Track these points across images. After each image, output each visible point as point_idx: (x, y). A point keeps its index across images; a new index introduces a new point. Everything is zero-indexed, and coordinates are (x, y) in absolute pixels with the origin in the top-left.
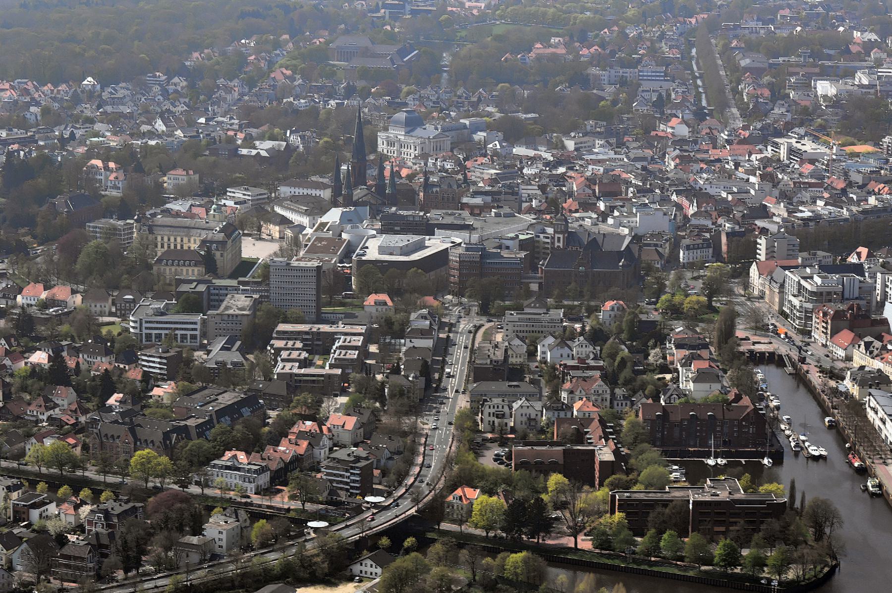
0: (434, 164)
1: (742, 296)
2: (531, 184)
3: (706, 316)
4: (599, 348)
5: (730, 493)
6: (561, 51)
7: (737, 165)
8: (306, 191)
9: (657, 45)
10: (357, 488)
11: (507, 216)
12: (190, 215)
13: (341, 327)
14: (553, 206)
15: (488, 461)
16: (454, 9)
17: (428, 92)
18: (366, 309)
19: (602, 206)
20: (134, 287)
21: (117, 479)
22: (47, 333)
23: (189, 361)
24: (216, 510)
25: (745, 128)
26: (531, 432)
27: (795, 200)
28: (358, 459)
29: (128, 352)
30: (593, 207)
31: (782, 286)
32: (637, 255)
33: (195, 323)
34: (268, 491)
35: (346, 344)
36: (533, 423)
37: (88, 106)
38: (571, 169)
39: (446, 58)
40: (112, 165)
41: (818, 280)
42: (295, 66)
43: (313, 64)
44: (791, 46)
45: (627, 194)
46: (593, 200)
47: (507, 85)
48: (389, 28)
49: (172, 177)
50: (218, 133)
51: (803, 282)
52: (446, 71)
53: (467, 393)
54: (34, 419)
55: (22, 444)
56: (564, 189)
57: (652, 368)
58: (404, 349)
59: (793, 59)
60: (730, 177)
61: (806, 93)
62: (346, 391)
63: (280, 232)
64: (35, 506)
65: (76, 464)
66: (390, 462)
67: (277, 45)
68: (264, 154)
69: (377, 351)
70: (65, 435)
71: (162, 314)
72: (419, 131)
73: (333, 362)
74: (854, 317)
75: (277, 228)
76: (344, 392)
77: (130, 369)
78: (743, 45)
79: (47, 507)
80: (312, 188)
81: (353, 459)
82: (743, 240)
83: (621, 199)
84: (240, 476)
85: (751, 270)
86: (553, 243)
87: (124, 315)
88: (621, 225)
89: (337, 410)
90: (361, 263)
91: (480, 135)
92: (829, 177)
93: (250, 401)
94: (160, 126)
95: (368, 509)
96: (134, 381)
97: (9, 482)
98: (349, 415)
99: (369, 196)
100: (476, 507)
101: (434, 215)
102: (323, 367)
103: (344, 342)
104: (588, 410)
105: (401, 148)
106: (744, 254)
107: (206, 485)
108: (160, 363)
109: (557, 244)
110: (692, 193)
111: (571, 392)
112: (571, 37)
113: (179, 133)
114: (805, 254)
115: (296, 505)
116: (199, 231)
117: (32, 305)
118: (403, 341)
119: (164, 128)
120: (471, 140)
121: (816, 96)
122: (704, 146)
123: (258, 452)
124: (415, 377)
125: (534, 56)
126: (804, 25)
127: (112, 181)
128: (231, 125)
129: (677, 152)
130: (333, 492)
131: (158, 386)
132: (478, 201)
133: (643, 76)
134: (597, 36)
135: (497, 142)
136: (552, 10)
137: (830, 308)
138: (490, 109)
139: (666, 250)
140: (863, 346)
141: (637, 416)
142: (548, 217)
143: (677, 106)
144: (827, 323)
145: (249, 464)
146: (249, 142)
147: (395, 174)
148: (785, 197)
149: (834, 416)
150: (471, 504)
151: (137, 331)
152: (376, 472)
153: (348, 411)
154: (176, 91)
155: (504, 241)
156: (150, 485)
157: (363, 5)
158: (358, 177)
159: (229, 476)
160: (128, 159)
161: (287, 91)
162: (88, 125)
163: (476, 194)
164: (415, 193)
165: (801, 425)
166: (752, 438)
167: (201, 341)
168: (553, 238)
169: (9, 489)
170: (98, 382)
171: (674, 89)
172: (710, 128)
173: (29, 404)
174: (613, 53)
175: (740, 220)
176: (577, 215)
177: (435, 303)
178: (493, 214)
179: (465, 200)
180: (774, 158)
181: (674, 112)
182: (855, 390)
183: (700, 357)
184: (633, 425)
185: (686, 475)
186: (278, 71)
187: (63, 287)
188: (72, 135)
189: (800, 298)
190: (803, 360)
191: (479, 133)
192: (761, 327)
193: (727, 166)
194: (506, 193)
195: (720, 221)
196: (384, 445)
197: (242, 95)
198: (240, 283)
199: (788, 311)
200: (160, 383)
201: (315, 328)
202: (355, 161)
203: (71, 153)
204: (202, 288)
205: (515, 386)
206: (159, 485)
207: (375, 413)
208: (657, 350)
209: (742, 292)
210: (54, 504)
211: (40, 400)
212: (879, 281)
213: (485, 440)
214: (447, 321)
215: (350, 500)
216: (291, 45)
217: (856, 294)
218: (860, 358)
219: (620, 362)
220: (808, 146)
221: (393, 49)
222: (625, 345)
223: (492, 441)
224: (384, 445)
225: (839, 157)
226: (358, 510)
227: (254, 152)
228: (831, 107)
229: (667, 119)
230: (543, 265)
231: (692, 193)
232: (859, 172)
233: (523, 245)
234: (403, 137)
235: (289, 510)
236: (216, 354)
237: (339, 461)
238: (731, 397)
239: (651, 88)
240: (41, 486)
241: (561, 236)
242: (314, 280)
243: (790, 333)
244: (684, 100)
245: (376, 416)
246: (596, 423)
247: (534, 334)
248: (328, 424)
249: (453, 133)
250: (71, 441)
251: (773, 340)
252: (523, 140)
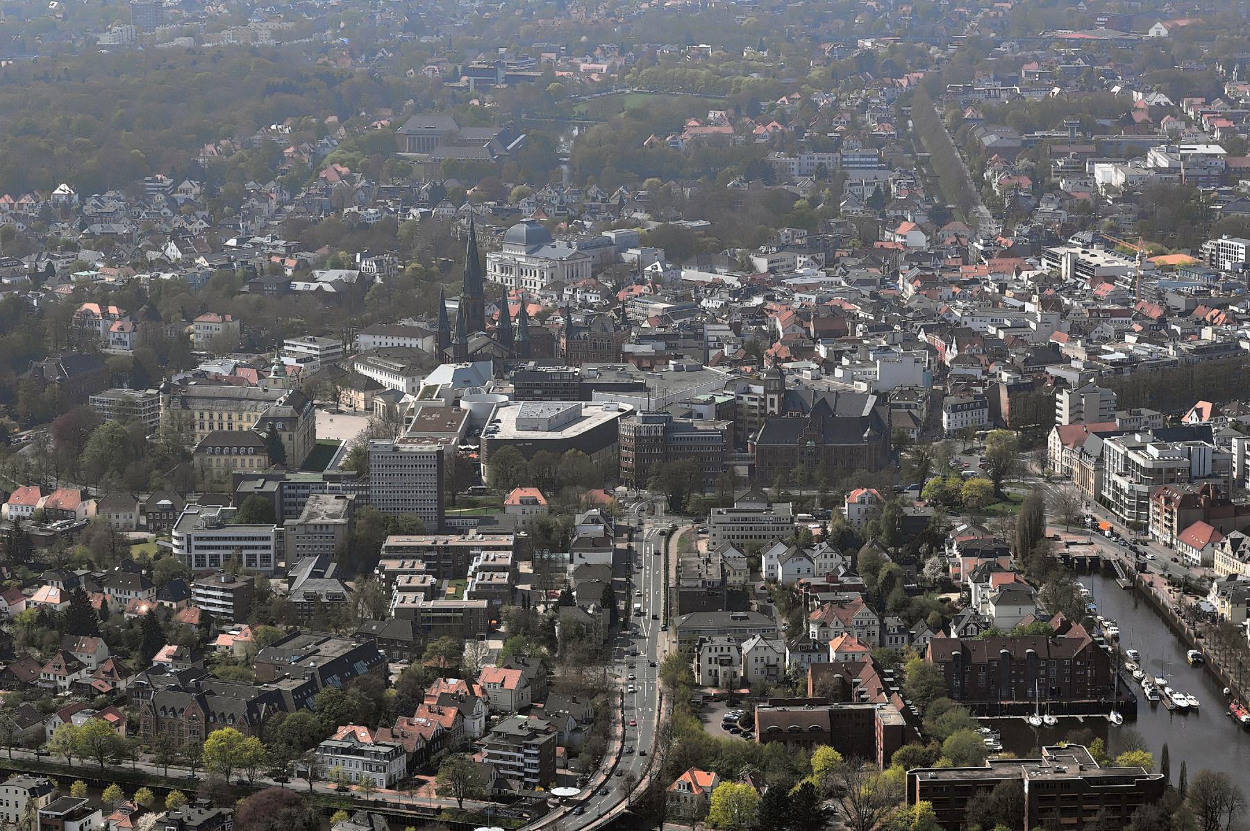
0: (572, 296)
1: (1039, 476)
2: (717, 323)
3: (992, 507)
4: (849, 558)
5: (1081, 768)
6: (727, 129)
7: (1003, 288)
8: (396, 341)
9: (859, 118)
10: (535, 776)
11: (690, 369)
12: (233, 380)
13: (473, 538)
14: (753, 353)
15: (715, 728)
16: (565, 73)
17: (546, 193)
18: (508, 510)
19: (822, 351)
20: (168, 487)
21: (186, 773)
22: (51, 559)
23: (264, 594)
24: (337, 815)
25: (1007, 233)
26: (776, 683)
27: (1093, 335)
28: (535, 733)
29: (174, 583)
30: (809, 353)
31: (1100, 460)
32: (886, 422)
33: (268, 538)
34: (405, 783)
35: (489, 562)
36: (773, 672)
37: (65, 225)
38: (770, 298)
39: (565, 147)
40: (113, 310)
41: (1153, 451)
42: (353, 160)
43: (377, 156)
44: (1050, 115)
45: (854, 333)
46: (809, 343)
47: (656, 179)
48: (476, 102)
49: (202, 325)
50: (257, 260)
51: (1131, 455)
52: (565, 163)
53: (671, 629)
54: (51, 686)
55: (40, 724)
56: (764, 327)
57: (928, 585)
58: (571, 568)
59: (1055, 134)
60: (995, 304)
61: (1083, 182)
62: (495, 632)
63: (366, 400)
64: (71, 817)
65: (122, 753)
66: (577, 735)
67: (323, 131)
68: (328, 288)
69: (531, 571)
70: (102, 709)
71: (219, 527)
72: (546, 251)
73: (474, 589)
74: (1211, 503)
75: (362, 395)
76: (492, 633)
77: (179, 610)
78: (981, 116)
79: (90, 817)
80: (405, 336)
81: (527, 733)
82: (1032, 395)
83: (849, 341)
84: (365, 763)
85: (1050, 439)
86: (764, 407)
87: (159, 528)
88: (853, 379)
89: (486, 660)
90: (495, 445)
91: (632, 254)
92: (1137, 303)
93: (367, 652)
94: (173, 252)
95: (557, 806)
96: (189, 625)
97: (33, 782)
98: (509, 667)
99: (491, 346)
100: (716, 799)
101: (586, 370)
102: (458, 597)
103: (487, 560)
104: (851, 649)
105: (523, 273)
106: (1034, 418)
107: (314, 778)
108: (223, 598)
109: (769, 409)
110: (949, 330)
111: (824, 625)
112: (737, 109)
113: (201, 261)
114: (1123, 414)
115: (451, 802)
116: (253, 403)
117: (24, 518)
118: (567, 556)
119: (179, 255)
120: (619, 260)
121: (1095, 185)
122: (950, 260)
123: (385, 726)
124: (597, 609)
125: (689, 138)
126: (1062, 85)
127: (117, 334)
128: (275, 247)
129: (916, 271)
130: (501, 782)
131: (224, 632)
132: (646, 348)
133: (848, 162)
134: (773, 107)
135: (658, 263)
136: (704, 72)
137: (1176, 491)
138: (638, 215)
139: (922, 414)
140: (1228, 545)
141: (922, 656)
142: (749, 369)
143: (902, 205)
144: (1171, 513)
145: (376, 744)
146: (304, 271)
147: (523, 315)
148: (1077, 331)
149: (1200, 649)
150: (706, 795)
151: (184, 552)
152: (560, 751)
153: (511, 659)
154: (188, 201)
155: (694, 407)
156: (234, 779)
157: (434, 71)
158: (473, 317)
159: (347, 762)
160: (133, 300)
161: (345, 198)
162: (70, 254)
163: (642, 339)
164: (551, 340)
165: (1154, 662)
166: (1092, 689)
167: (276, 564)
168: (764, 400)
169: (34, 792)
170: (138, 628)
171: (895, 181)
172: (956, 235)
173: (42, 665)
174: (800, 131)
175: (1022, 367)
176: (789, 365)
177: (608, 500)
178: (671, 368)
179: (628, 348)
180: (1052, 276)
181: (899, 213)
182: (1225, 610)
183: (999, 568)
184: (923, 672)
185: (1001, 740)
186: (330, 168)
187: (69, 491)
188: (50, 269)
189: (1129, 478)
190: (1142, 568)
191: (630, 251)
192: (1075, 522)
193: (986, 289)
194: (686, 337)
195: (993, 368)
196: (566, 710)
197: (282, 204)
198: (326, 478)
199: (1110, 497)
200: (225, 627)
201: (441, 540)
202: (468, 296)
203: (51, 294)
204: (272, 487)
205: (742, 618)
206: (246, 779)
207: (545, 663)
208: (935, 559)
209: (1039, 471)
210: (100, 812)
211: (59, 659)
212: (1235, 450)
213: (707, 697)
214: (624, 523)
215: (526, 793)
216: (342, 131)
217: (1208, 471)
218: (1224, 564)
219: (887, 578)
220: (1100, 258)
221: (492, 133)
222: (888, 552)
223: (718, 698)
224: (566, 710)
225: (1148, 273)
226: (541, 809)
227: (314, 286)
228: (1123, 200)
229: (896, 223)
230: (754, 439)
231: (949, 330)
232: (1180, 293)
233: (723, 411)
234: (523, 260)
235: (439, 811)
236: (303, 581)
237: (508, 737)
238: (1056, 624)
239: (863, 181)
240: (78, 787)
241: (776, 397)
242: (434, 470)
243: (1116, 529)
244: (912, 195)
245: (546, 667)
246: (869, 670)
247: (753, 540)
248: (480, 681)
249: (595, 252)
250: (112, 718)
251: (1094, 540)
252: (694, 259)
